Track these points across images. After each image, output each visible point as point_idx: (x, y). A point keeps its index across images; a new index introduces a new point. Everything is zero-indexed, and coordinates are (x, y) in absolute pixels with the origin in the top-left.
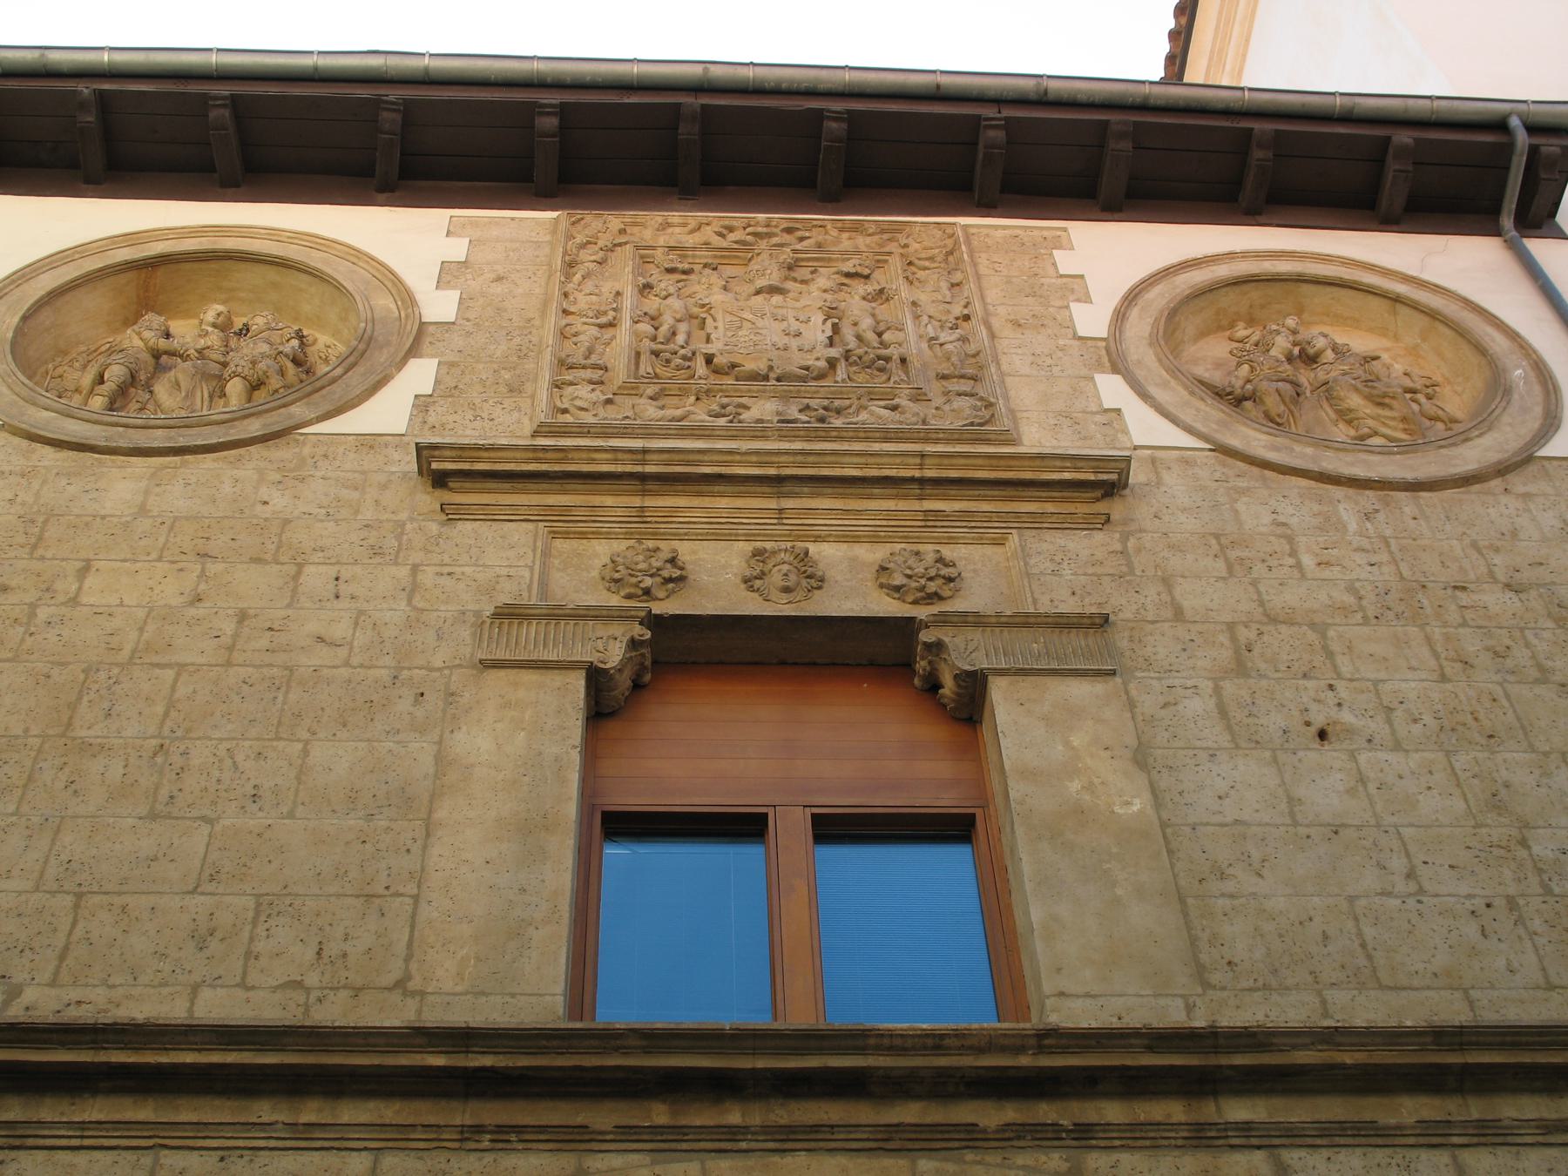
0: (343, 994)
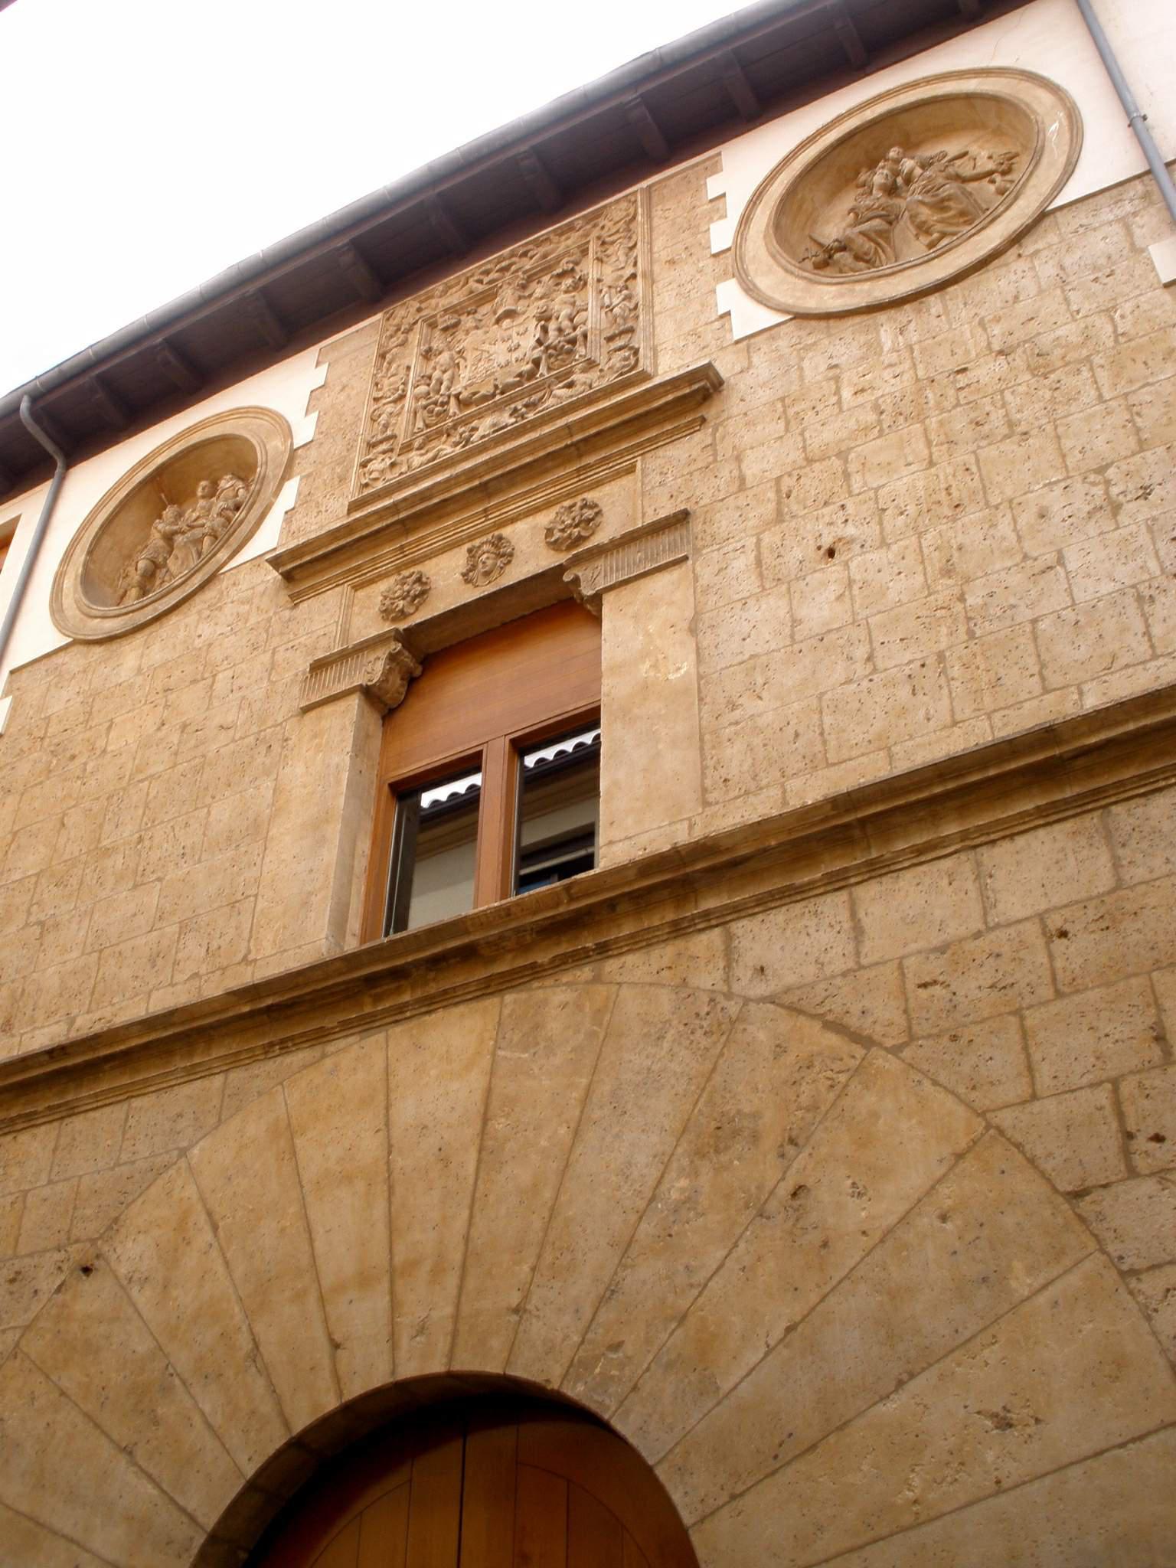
0: (218, 973)
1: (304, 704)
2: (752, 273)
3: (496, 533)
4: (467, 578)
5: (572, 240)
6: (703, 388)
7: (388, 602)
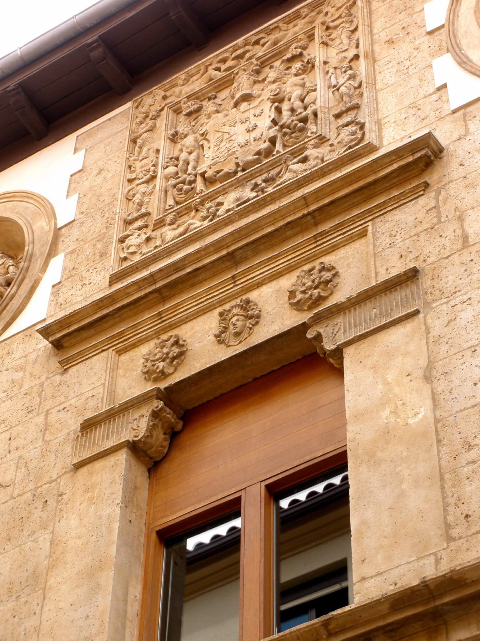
1: (76, 461)
2: (464, 47)
3: (244, 297)
4: (220, 339)
5: (300, 26)
6: (425, 155)
7: (149, 364)
